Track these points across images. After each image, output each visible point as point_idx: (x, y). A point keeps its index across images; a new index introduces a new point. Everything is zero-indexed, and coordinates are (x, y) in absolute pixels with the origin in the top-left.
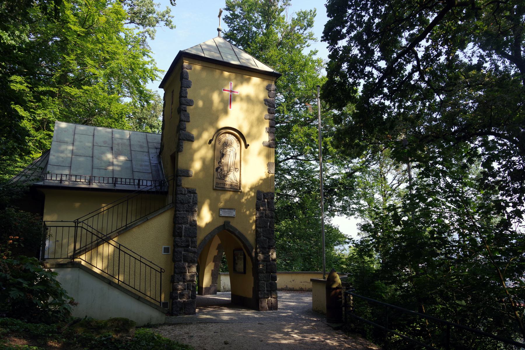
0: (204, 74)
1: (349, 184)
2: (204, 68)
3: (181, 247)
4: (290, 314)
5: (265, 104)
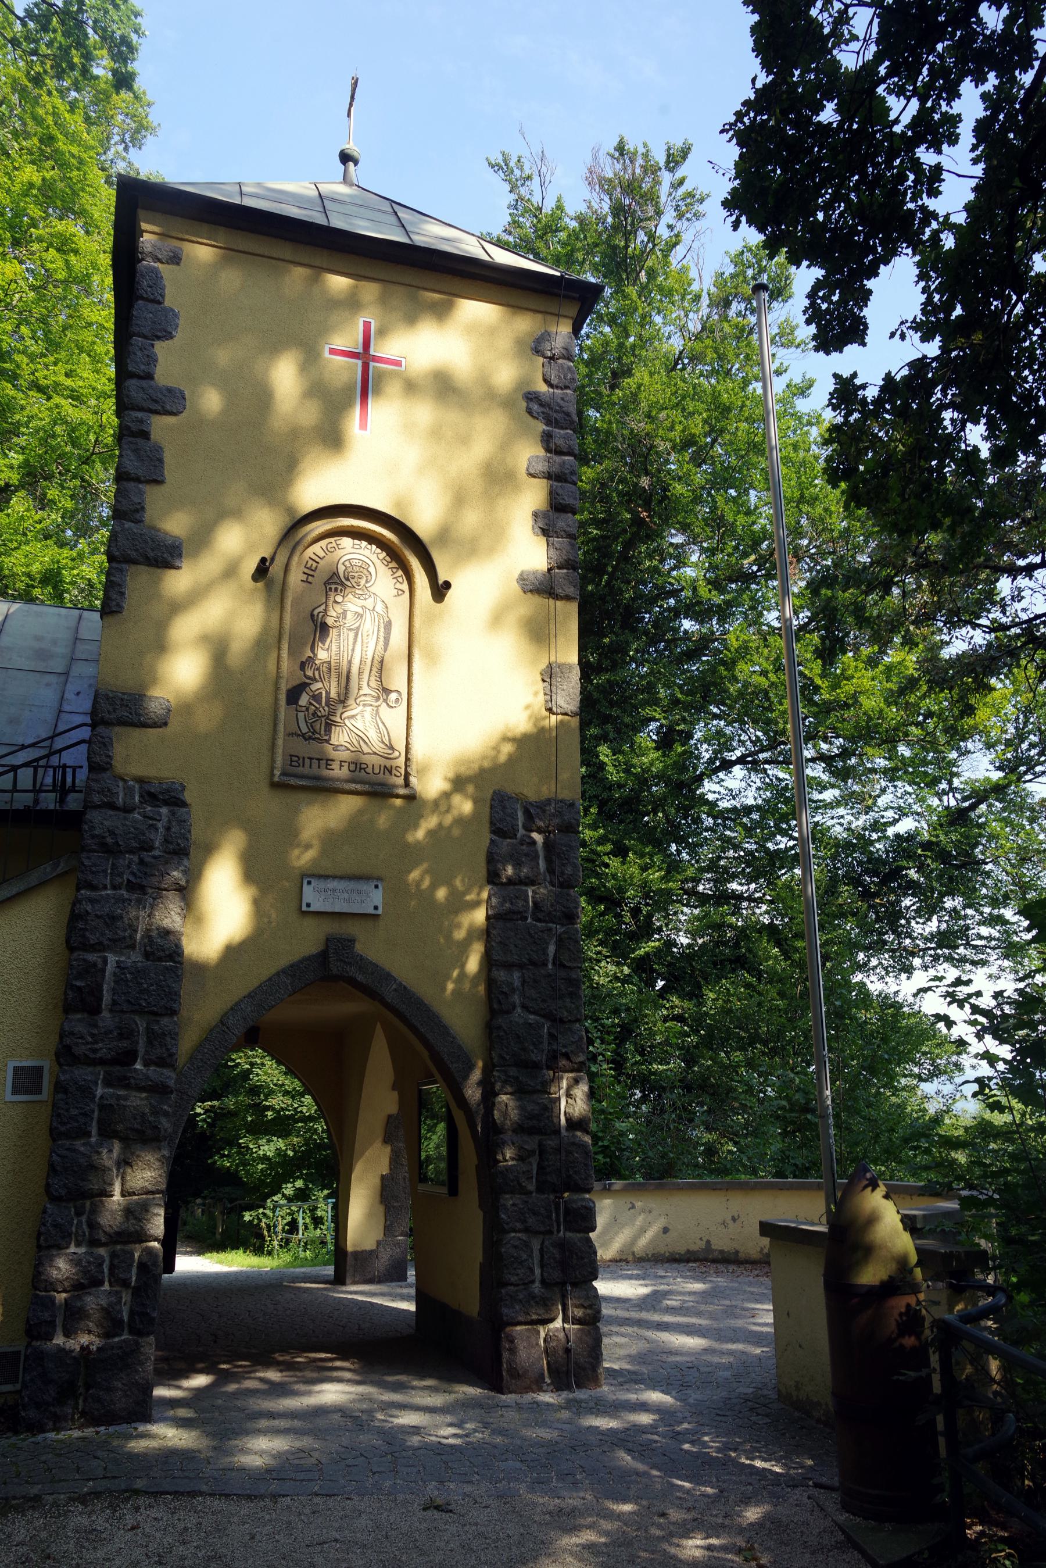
0: (231, 279)
1: (957, 844)
2: (231, 254)
3: (94, 1063)
4: (645, 1419)
5: (529, 412)
